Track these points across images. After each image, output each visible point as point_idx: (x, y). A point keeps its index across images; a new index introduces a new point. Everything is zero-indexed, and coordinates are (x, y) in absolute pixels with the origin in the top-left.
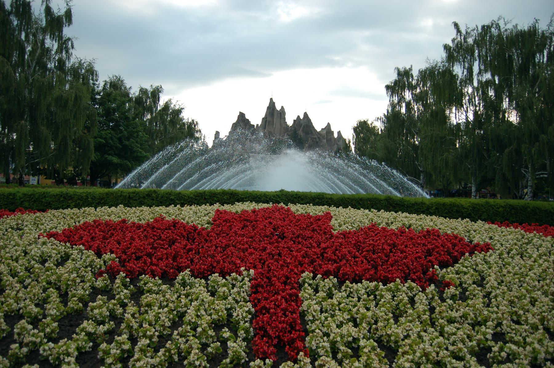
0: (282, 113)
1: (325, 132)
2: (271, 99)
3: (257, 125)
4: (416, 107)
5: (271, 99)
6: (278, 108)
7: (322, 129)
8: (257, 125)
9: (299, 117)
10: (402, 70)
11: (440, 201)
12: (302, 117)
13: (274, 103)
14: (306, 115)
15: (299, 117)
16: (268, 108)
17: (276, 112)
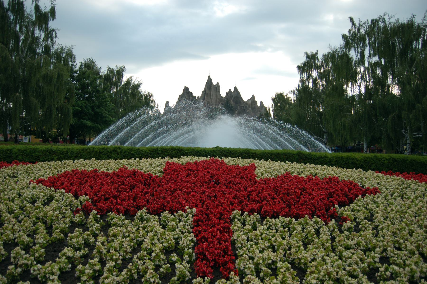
0: (217, 87)
1: (250, 102)
2: (209, 77)
3: (198, 96)
4: (320, 82)
5: (209, 77)
6: (214, 83)
7: (248, 100)
8: (198, 96)
9: (230, 90)
10: (310, 54)
11: (339, 155)
12: (232, 90)
13: (211, 80)
14: (236, 89)
15: (230, 90)
16: (207, 83)
17: (212, 86)
